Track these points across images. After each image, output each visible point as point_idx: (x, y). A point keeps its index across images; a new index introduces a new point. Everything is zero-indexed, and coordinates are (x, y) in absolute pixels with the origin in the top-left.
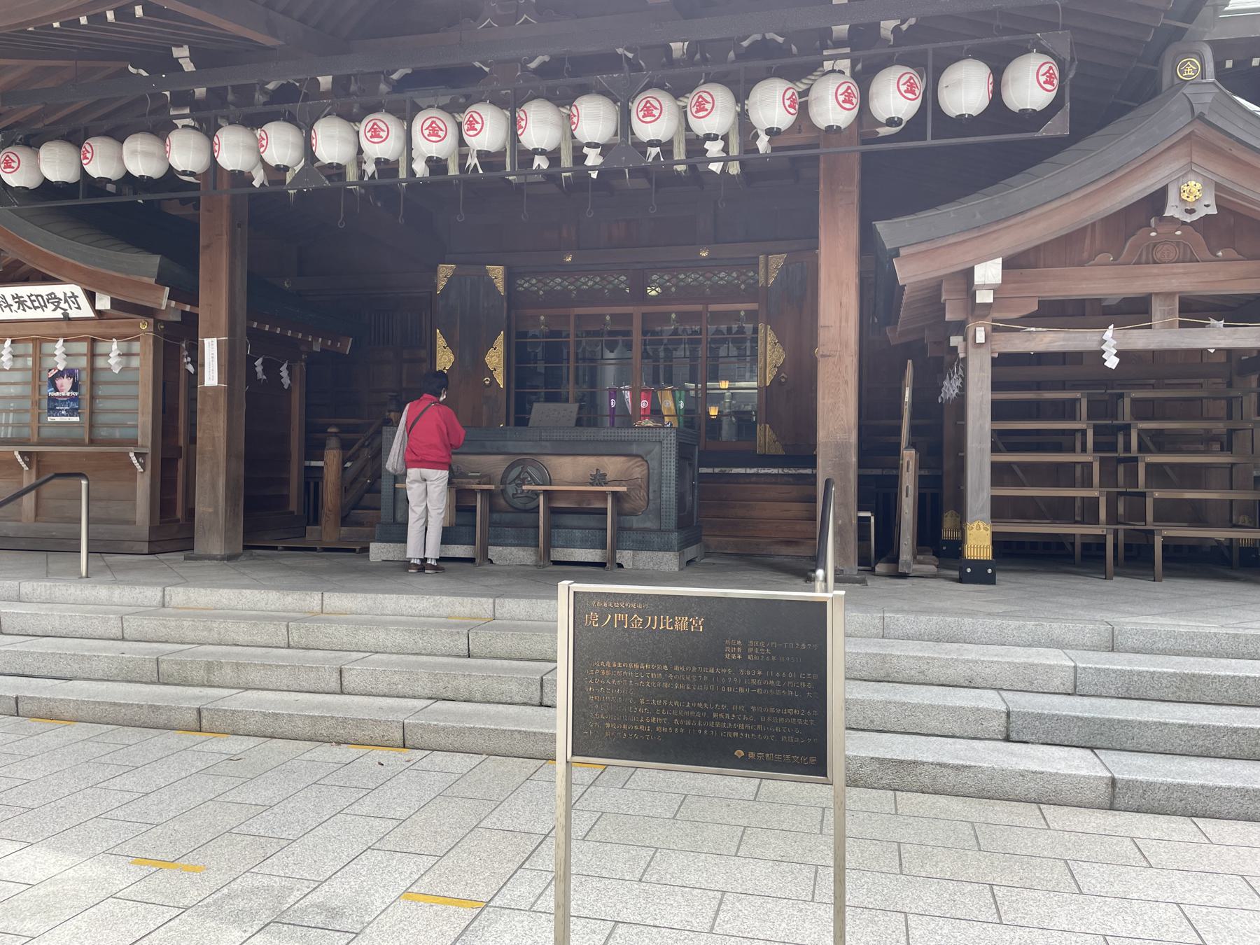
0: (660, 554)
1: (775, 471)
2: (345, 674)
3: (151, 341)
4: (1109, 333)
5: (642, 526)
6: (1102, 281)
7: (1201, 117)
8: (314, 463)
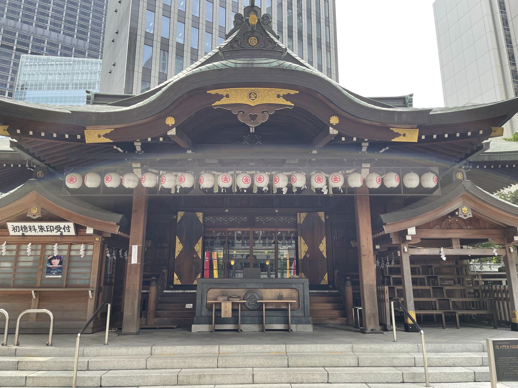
0: (306, 325)
1: (315, 291)
2: (255, 376)
3: (99, 245)
4: (442, 249)
5: (297, 315)
6: (436, 234)
7: (467, 191)
8: (145, 291)
